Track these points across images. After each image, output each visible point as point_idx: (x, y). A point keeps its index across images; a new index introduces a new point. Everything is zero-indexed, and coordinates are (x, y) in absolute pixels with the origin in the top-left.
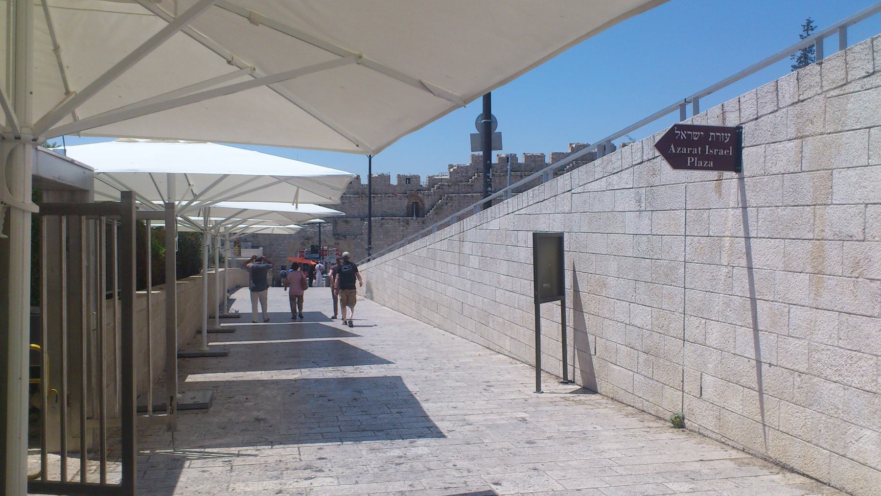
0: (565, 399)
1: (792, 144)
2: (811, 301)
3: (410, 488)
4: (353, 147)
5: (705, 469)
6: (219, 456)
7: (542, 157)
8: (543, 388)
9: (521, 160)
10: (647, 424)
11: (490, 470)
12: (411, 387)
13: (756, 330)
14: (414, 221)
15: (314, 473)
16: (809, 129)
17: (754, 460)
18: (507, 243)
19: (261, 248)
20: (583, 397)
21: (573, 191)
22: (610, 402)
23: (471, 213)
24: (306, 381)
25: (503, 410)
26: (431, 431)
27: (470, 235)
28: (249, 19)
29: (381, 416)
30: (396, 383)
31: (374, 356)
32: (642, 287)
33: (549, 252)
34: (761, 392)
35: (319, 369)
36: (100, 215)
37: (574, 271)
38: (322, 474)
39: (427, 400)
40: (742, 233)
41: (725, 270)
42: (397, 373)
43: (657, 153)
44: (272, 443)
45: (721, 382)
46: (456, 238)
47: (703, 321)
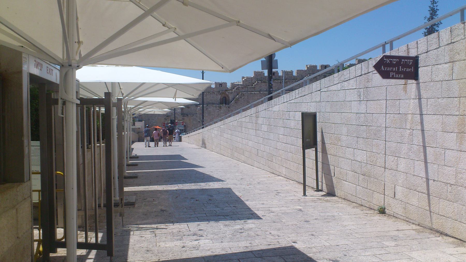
0: (320, 199)
1: (447, 65)
2: (457, 147)
3: (250, 245)
4: (220, 68)
5: (400, 234)
6: (147, 229)
7: (292, 72)
8: (307, 194)
9: (295, 74)
10: (365, 212)
11: (290, 236)
12: (237, 194)
13: (426, 162)
14: (224, 107)
15: (198, 237)
16: (457, 57)
17: (425, 230)
18: (283, 118)
19: (143, 122)
20: (328, 198)
21: (321, 91)
22: (343, 200)
23: (262, 102)
24: (182, 191)
25: (288, 205)
26: (253, 216)
27: (262, 114)
28: (183, 3)
29: (226, 208)
30: (228, 192)
31: (214, 178)
32: (361, 141)
33: (309, 121)
34: (429, 195)
35: (187, 184)
36: (94, 105)
37: (322, 132)
38: (203, 238)
39: (247, 200)
40: (418, 112)
41: (409, 131)
42: (228, 186)
43: (374, 69)
44: (173, 222)
45: (406, 190)
46: (254, 115)
47: (396, 158)
